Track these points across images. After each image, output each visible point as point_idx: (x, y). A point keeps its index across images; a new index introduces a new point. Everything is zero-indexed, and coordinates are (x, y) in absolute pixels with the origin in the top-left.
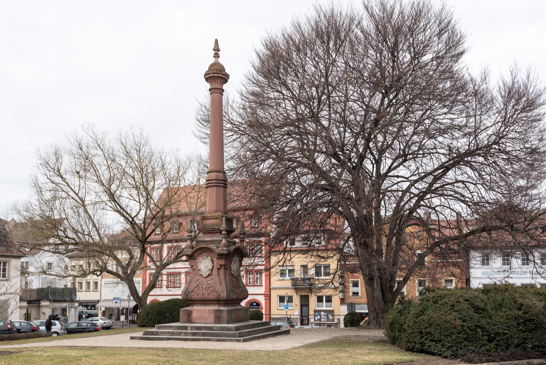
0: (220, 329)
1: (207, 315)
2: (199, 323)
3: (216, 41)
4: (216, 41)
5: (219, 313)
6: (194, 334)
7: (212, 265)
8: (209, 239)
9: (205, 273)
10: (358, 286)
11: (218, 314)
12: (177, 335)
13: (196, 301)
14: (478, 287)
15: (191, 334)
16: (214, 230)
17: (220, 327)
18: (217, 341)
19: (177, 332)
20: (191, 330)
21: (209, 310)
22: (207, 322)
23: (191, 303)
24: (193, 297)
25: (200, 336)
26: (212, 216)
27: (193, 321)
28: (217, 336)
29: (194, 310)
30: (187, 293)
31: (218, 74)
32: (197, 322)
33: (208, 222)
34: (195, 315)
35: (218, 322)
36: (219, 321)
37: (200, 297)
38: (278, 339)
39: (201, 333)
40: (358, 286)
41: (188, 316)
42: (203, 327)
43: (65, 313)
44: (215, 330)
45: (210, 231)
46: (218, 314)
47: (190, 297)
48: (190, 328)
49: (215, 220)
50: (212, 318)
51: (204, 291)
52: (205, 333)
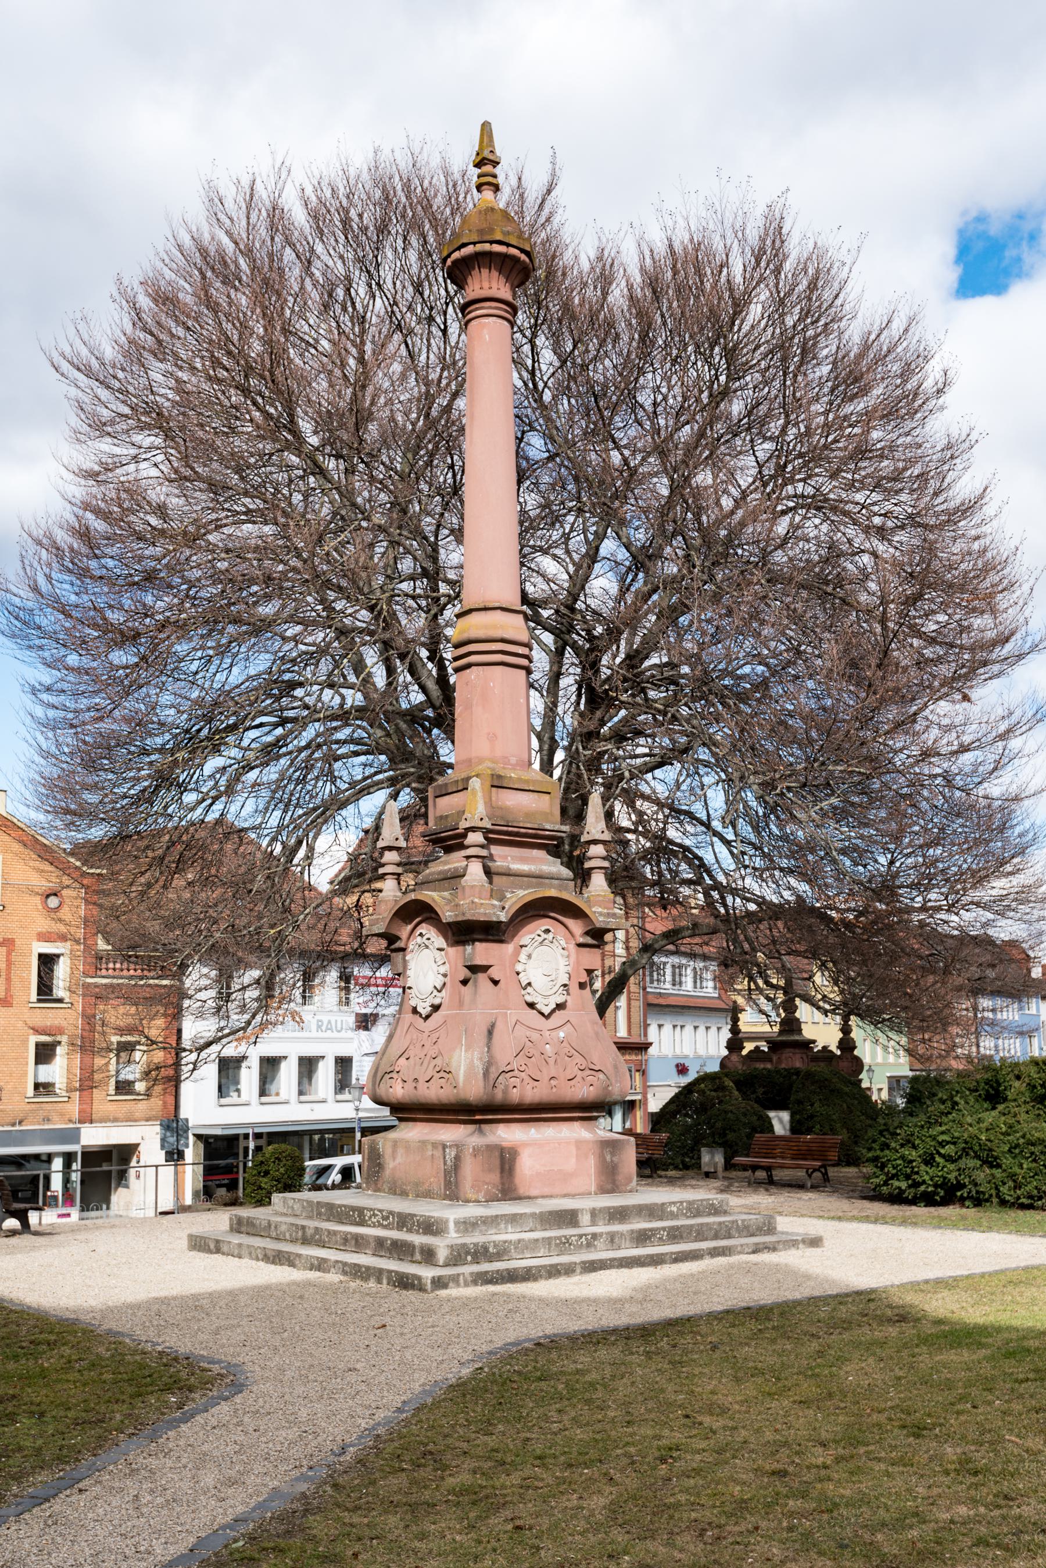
0: (689, 1209)
1: (571, 1164)
2: (565, 1196)
3: (486, 129)
4: (486, 129)
5: (613, 1154)
8: (525, 868)
9: (546, 996)
11: (608, 1158)
14: (1020, 1001)
15: (632, 1239)
17: (690, 1203)
21: (579, 1143)
26: (527, 782)
27: (522, 1191)
28: (716, 1237)
29: (525, 1145)
30: (493, 1076)
31: (508, 245)
32: (533, 1192)
33: (512, 800)
34: (527, 1165)
35: (609, 1186)
36: (614, 1182)
39: (664, 1229)
41: (502, 1170)
43: (712, 1158)
44: (673, 1216)
46: (608, 1158)
47: (505, 1092)
52: (678, 1228)
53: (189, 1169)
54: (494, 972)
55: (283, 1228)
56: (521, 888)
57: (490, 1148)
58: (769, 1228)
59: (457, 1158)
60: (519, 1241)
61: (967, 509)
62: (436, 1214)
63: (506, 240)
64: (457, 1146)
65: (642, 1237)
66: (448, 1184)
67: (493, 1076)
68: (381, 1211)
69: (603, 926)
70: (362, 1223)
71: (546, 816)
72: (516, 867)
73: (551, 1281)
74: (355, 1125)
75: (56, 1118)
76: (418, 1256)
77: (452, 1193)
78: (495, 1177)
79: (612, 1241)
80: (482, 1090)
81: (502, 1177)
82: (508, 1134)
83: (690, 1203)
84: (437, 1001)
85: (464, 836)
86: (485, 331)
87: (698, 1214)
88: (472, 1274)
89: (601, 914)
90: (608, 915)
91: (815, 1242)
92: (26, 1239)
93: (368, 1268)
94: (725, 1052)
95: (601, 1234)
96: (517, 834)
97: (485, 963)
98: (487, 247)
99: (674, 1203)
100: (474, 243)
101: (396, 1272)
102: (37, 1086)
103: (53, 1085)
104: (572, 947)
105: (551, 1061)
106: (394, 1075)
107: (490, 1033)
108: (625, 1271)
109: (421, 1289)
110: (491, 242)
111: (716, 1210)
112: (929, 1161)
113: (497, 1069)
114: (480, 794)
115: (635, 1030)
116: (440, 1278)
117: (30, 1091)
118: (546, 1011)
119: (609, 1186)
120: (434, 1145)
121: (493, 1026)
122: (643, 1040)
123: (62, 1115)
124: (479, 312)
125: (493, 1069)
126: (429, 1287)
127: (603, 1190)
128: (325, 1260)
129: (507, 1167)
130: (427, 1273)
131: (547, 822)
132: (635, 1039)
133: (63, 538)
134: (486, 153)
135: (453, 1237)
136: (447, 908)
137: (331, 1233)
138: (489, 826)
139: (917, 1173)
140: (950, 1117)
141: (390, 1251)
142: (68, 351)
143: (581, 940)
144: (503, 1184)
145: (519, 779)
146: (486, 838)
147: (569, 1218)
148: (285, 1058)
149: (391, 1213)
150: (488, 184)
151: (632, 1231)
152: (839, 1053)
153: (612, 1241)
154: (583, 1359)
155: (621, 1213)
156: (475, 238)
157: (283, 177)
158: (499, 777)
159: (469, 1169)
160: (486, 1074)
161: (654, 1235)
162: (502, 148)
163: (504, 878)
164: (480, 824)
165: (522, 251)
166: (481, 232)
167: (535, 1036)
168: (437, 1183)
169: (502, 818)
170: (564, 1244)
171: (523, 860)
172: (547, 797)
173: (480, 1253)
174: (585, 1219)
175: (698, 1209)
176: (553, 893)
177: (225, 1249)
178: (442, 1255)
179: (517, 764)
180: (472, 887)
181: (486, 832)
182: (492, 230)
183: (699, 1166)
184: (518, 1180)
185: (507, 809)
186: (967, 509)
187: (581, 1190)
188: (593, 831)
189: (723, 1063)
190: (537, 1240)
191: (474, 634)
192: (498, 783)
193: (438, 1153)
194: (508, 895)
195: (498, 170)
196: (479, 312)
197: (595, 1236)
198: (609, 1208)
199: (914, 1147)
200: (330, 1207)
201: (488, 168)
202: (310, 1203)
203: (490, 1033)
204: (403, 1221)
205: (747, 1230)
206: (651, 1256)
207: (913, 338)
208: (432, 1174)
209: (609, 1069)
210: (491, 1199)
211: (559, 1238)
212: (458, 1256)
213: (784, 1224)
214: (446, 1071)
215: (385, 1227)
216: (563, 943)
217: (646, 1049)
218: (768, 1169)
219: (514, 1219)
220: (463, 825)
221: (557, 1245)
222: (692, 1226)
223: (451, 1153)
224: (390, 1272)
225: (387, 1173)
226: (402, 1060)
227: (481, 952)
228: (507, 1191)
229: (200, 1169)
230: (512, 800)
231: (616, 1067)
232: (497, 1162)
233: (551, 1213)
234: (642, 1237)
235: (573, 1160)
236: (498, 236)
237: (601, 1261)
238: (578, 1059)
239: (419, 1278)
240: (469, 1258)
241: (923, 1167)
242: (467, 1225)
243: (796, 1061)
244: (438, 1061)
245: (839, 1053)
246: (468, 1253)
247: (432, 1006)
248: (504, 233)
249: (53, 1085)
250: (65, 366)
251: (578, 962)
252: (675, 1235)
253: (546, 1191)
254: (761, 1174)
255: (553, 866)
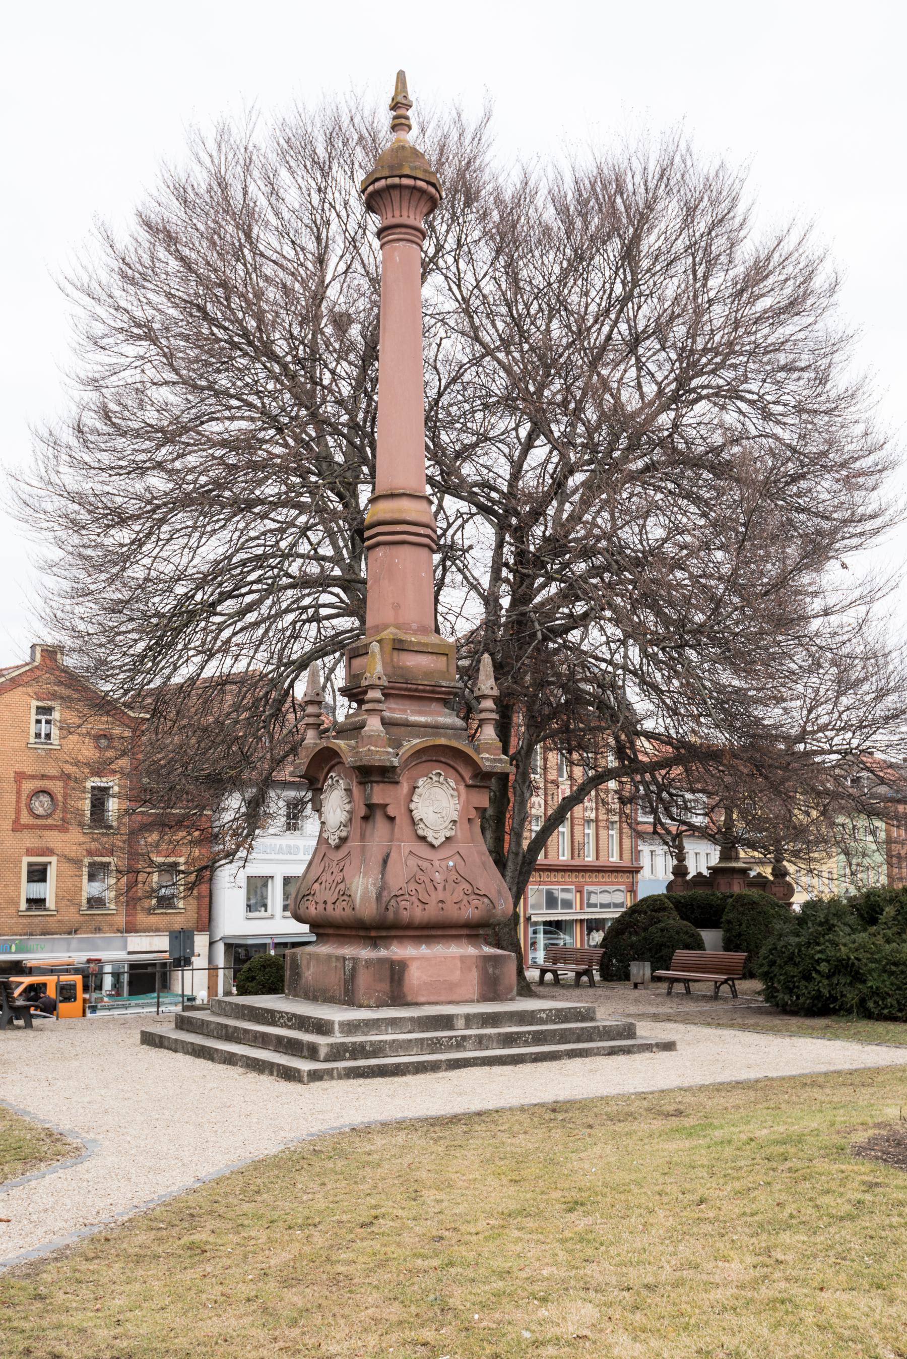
0: (557, 1016)
1: (456, 976)
2: (450, 1003)
3: (401, 78)
4: (401, 78)
5: (495, 967)
6: (481, 1042)
7: (412, 806)
8: (422, 719)
10: (43, 879)
11: (491, 971)
12: (450, 1048)
13: (409, 926)
15: (498, 1042)
16: (433, 692)
17: (557, 1010)
18: (609, 1054)
19: (451, 1038)
20: (468, 1027)
21: (463, 959)
22: (455, 997)
23: (384, 934)
24: (405, 915)
25: (527, 1044)
26: (426, 645)
27: (409, 999)
28: (578, 1040)
29: (413, 959)
30: (385, 898)
31: (415, 178)
32: (422, 999)
33: (412, 661)
34: (415, 976)
35: (491, 995)
36: (495, 992)
37: (431, 912)
38: (161, 1055)
39: (529, 1033)
40: (43, 879)
41: (392, 979)
42: (506, 1013)
43: (641, 970)
44: (542, 1022)
45: (424, 691)
47: (396, 913)
48: (461, 1023)
49: (434, 657)
50: (472, 982)
51: (441, 895)
52: (542, 1032)
53: (221, 973)
54: (391, 811)
55: (212, 1026)
56: (418, 737)
57: (381, 961)
58: (629, 1032)
59: (354, 969)
60: (394, 1041)
61: (851, 396)
62: (326, 1017)
63: (413, 174)
64: (353, 959)
65: (509, 1040)
66: (347, 992)
67: (385, 898)
68: (287, 1013)
69: (489, 769)
70: (273, 1023)
71: (445, 674)
72: (414, 718)
73: (418, 1076)
74: (268, 941)
75: (106, 928)
76: (306, 1053)
77: (349, 999)
78: (385, 986)
79: (480, 1042)
80: (375, 911)
81: (391, 986)
82: (398, 951)
83: (559, 1011)
84: (344, 834)
85: (365, 692)
86: (396, 254)
87: (566, 1020)
88: (345, 1068)
89: (487, 759)
90: (495, 760)
91: (669, 1046)
92: (30, 1033)
93: (264, 1061)
94: (672, 877)
95: (470, 1037)
96: (416, 690)
97: (381, 802)
98: (396, 180)
99: (544, 1011)
100: (386, 178)
101: (283, 1066)
102: (29, 901)
103: (43, 901)
104: (462, 788)
105: (439, 887)
106: (310, 898)
107: (385, 862)
108: (487, 1068)
109: (300, 1081)
110: (400, 177)
111: (587, 1015)
112: (807, 978)
113: (389, 892)
114: (378, 656)
115: (627, 855)
116: (315, 1071)
117: (23, 905)
118: (436, 843)
119: (491, 995)
120: (338, 958)
121: (388, 856)
122: (635, 865)
123: (111, 925)
124: (390, 237)
125: (385, 893)
126: (305, 1079)
127: (485, 998)
128: (234, 1055)
129: (396, 977)
130: (305, 1066)
131: (444, 679)
132: (626, 863)
133: (68, 437)
134: (400, 98)
135: (338, 1038)
136: (350, 754)
137: (246, 1031)
138: (386, 684)
139: (798, 987)
140: (827, 937)
141: (286, 1047)
142: (72, 276)
143: (470, 782)
144: (392, 992)
145: (419, 643)
146: (383, 694)
147: (447, 1022)
148: (272, 877)
149: (294, 1015)
150: (400, 124)
151: (499, 1034)
152: (771, 878)
153: (480, 1042)
154: (380, 1141)
155: (493, 1019)
156: (386, 173)
157: (253, 119)
158: (400, 641)
159: (363, 979)
160: (379, 897)
161: (520, 1038)
162: (413, 93)
163: (403, 728)
164: (378, 682)
165: (428, 183)
166: (391, 168)
167: (425, 865)
168: (338, 991)
169: (402, 676)
170: (435, 1045)
171: (421, 713)
172: (445, 658)
173: (358, 1051)
174: (461, 1023)
175: (566, 1016)
176: (443, 741)
177: (166, 1044)
178: (323, 1052)
179: (418, 630)
180: (370, 736)
181: (383, 689)
182: (400, 166)
183: (627, 977)
184: (406, 989)
185: (407, 669)
186: (851, 396)
187: (467, 998)
188: (483, 687)
189: (670, 886)
190: (410, 1041)
191: (388, 516)
192: (400, 646)
193: (340, 965)
194: (405, 743)
195: (409, 113)
196: (390, 237)
197: (464, 1038)
198: (482, 1014)
199: (795, 964)
200: (251, 1009)
201: (401, 112)
202: (237, 1005)
203: (385, 862)
204: (302, 1023)
205: (607, 1033)
206: (513, 1056)
207: (807, 246)
208: (334, 981)
209: (493, 894)
210: (380, 1005)
211: (431, 1039)
212: (337, 1053)
213: (646, 1031)
214: (346, 895)
215: (289, 1027)
216: (453, 784)
217: (638, 872)
218: (686, 981)
219: (394, 1023)
220: (364, 683)
221: (428, 1045)
222: (555, 1030)
223: (349, 965)
224: (279, 1065)
225: (303, 980)
226: (316, 885)
227: (379, 793)
228: (397, 998)
229: (231, 973)
230: (412, 661)
231: (499, 892)
232: (388, 973)
233: (428, 1017)
234: (509, 1040)
235: (458, 972)
236: (407, 171)
237: (465, 1059)
238: (466, 886)
239: (298, 1071)
240: (347, 1055)
241: (803, 983)
242: (350, 1027)
243: (737, 888)
244: (342, 886)
245: (771, 878)
246: (346, 1051)
247: (340, 838)
248: (411, 169)
249: (43, 901)
250: (70, 289)
251: (468, 801)
252: (539, 1038)
253: (433, 999)
254: (679, 988)
255: (448, 718)
